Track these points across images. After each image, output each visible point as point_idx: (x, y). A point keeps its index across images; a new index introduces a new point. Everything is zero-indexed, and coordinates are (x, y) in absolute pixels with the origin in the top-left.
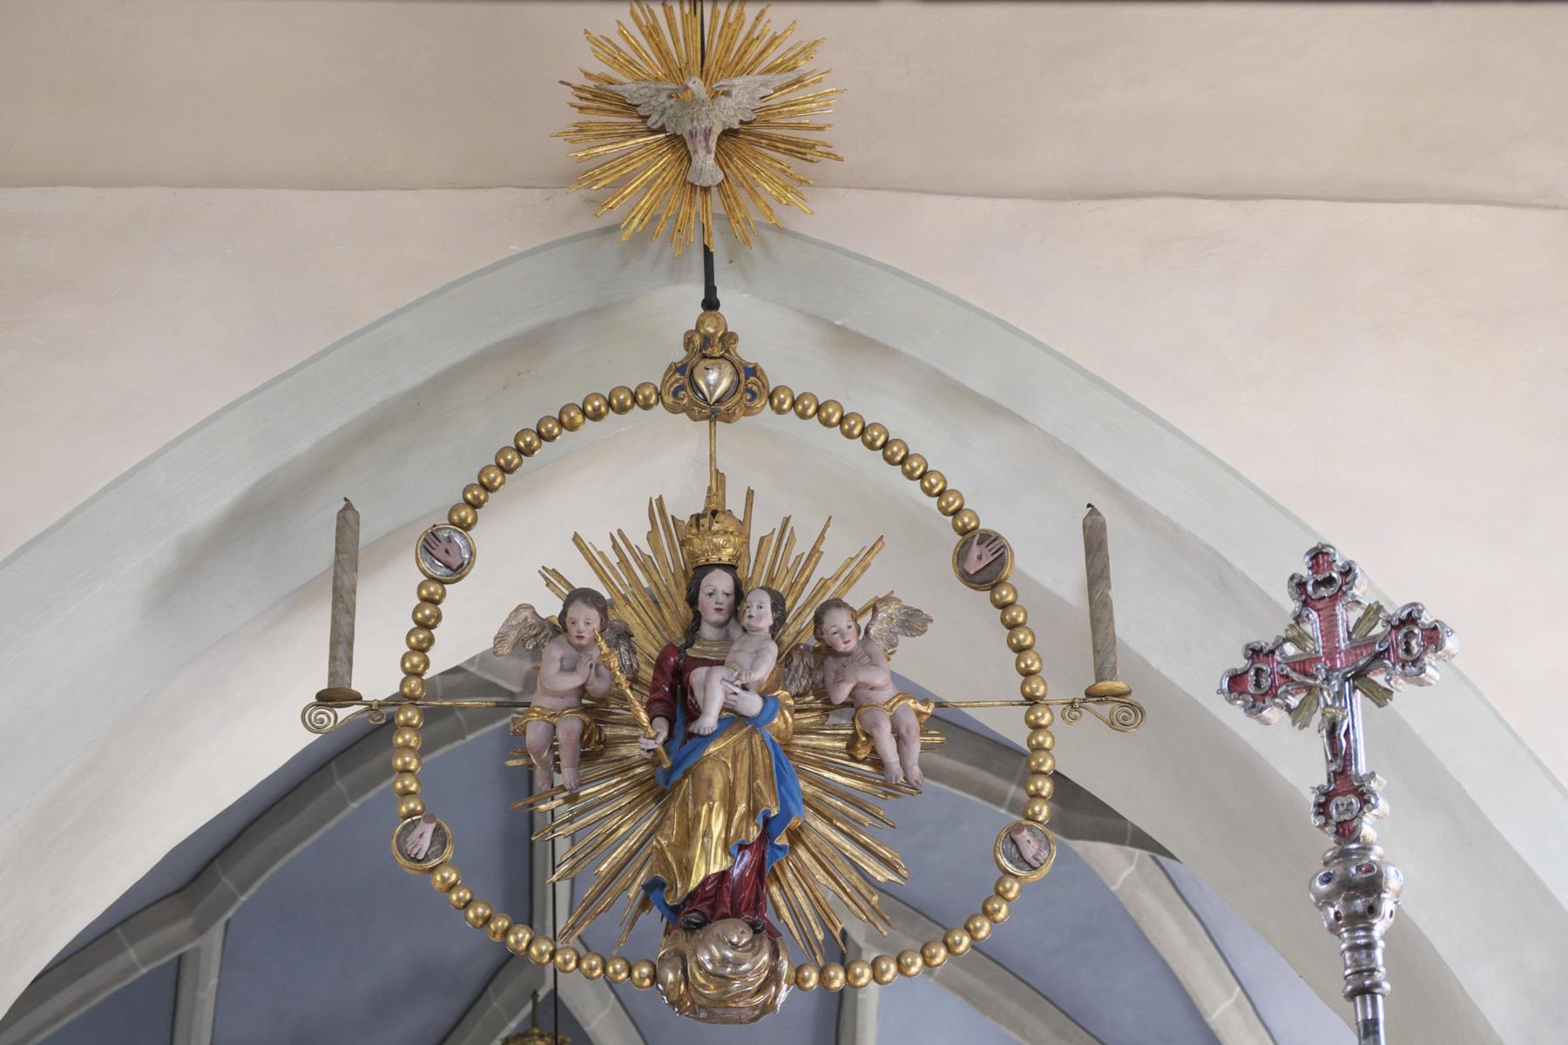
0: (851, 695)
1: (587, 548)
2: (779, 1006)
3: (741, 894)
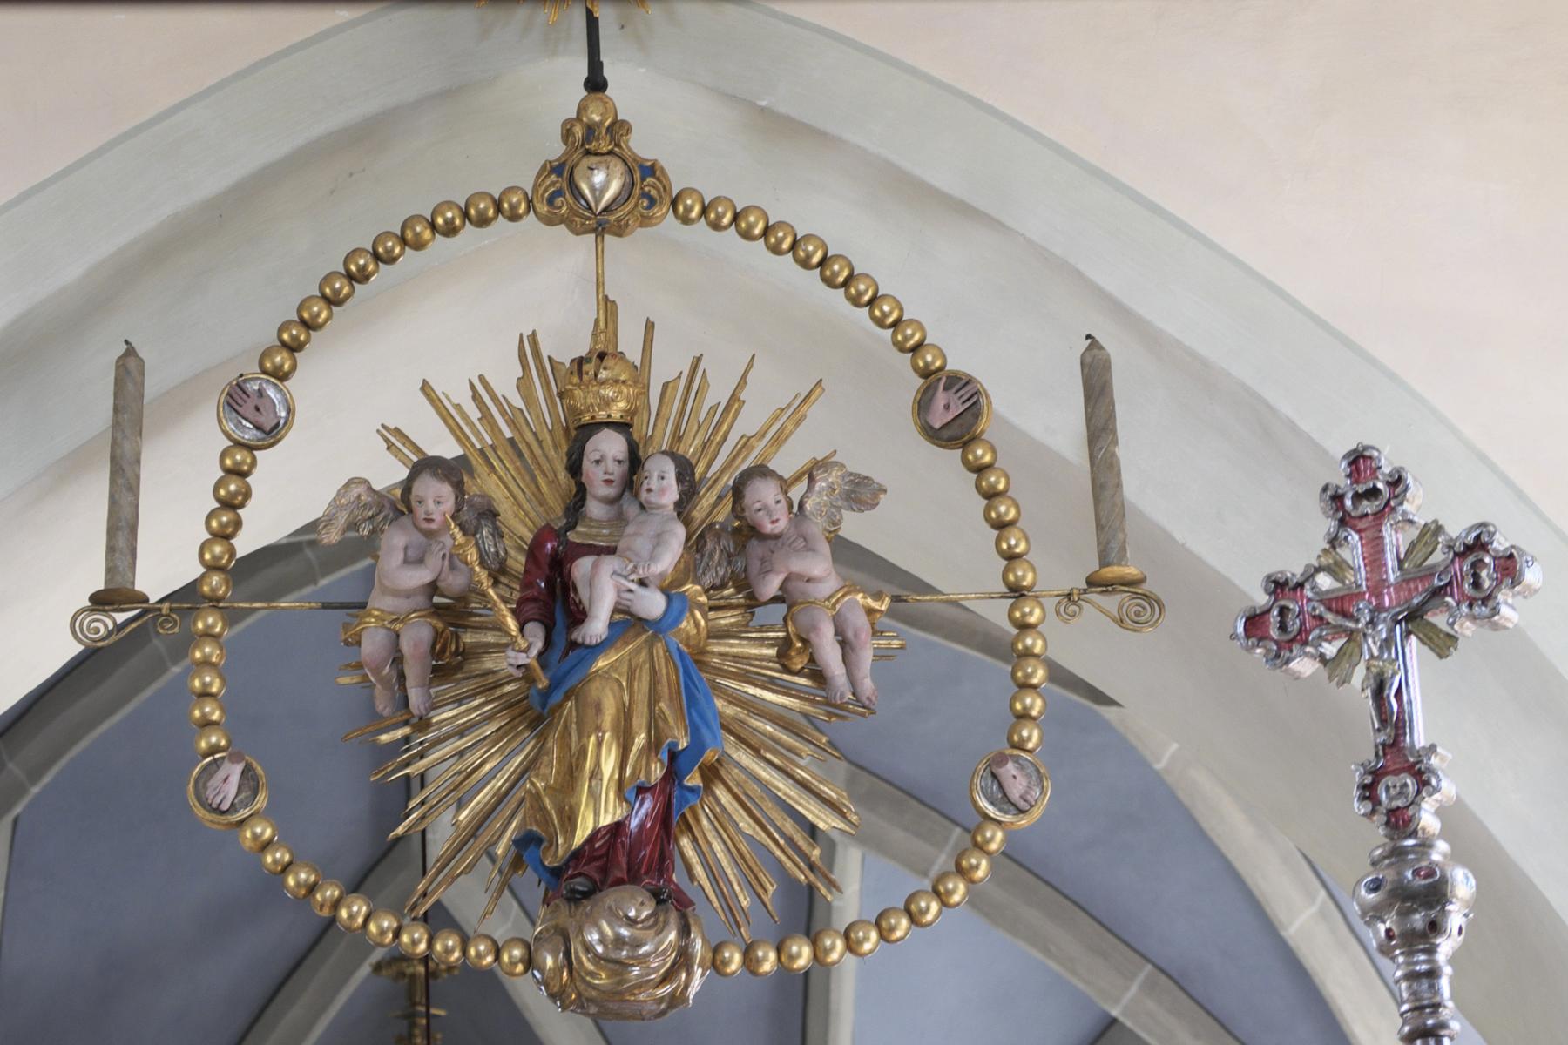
0: (781, 588)
1: (440, 400)
2: (691, 997)
3: (640, 851)
